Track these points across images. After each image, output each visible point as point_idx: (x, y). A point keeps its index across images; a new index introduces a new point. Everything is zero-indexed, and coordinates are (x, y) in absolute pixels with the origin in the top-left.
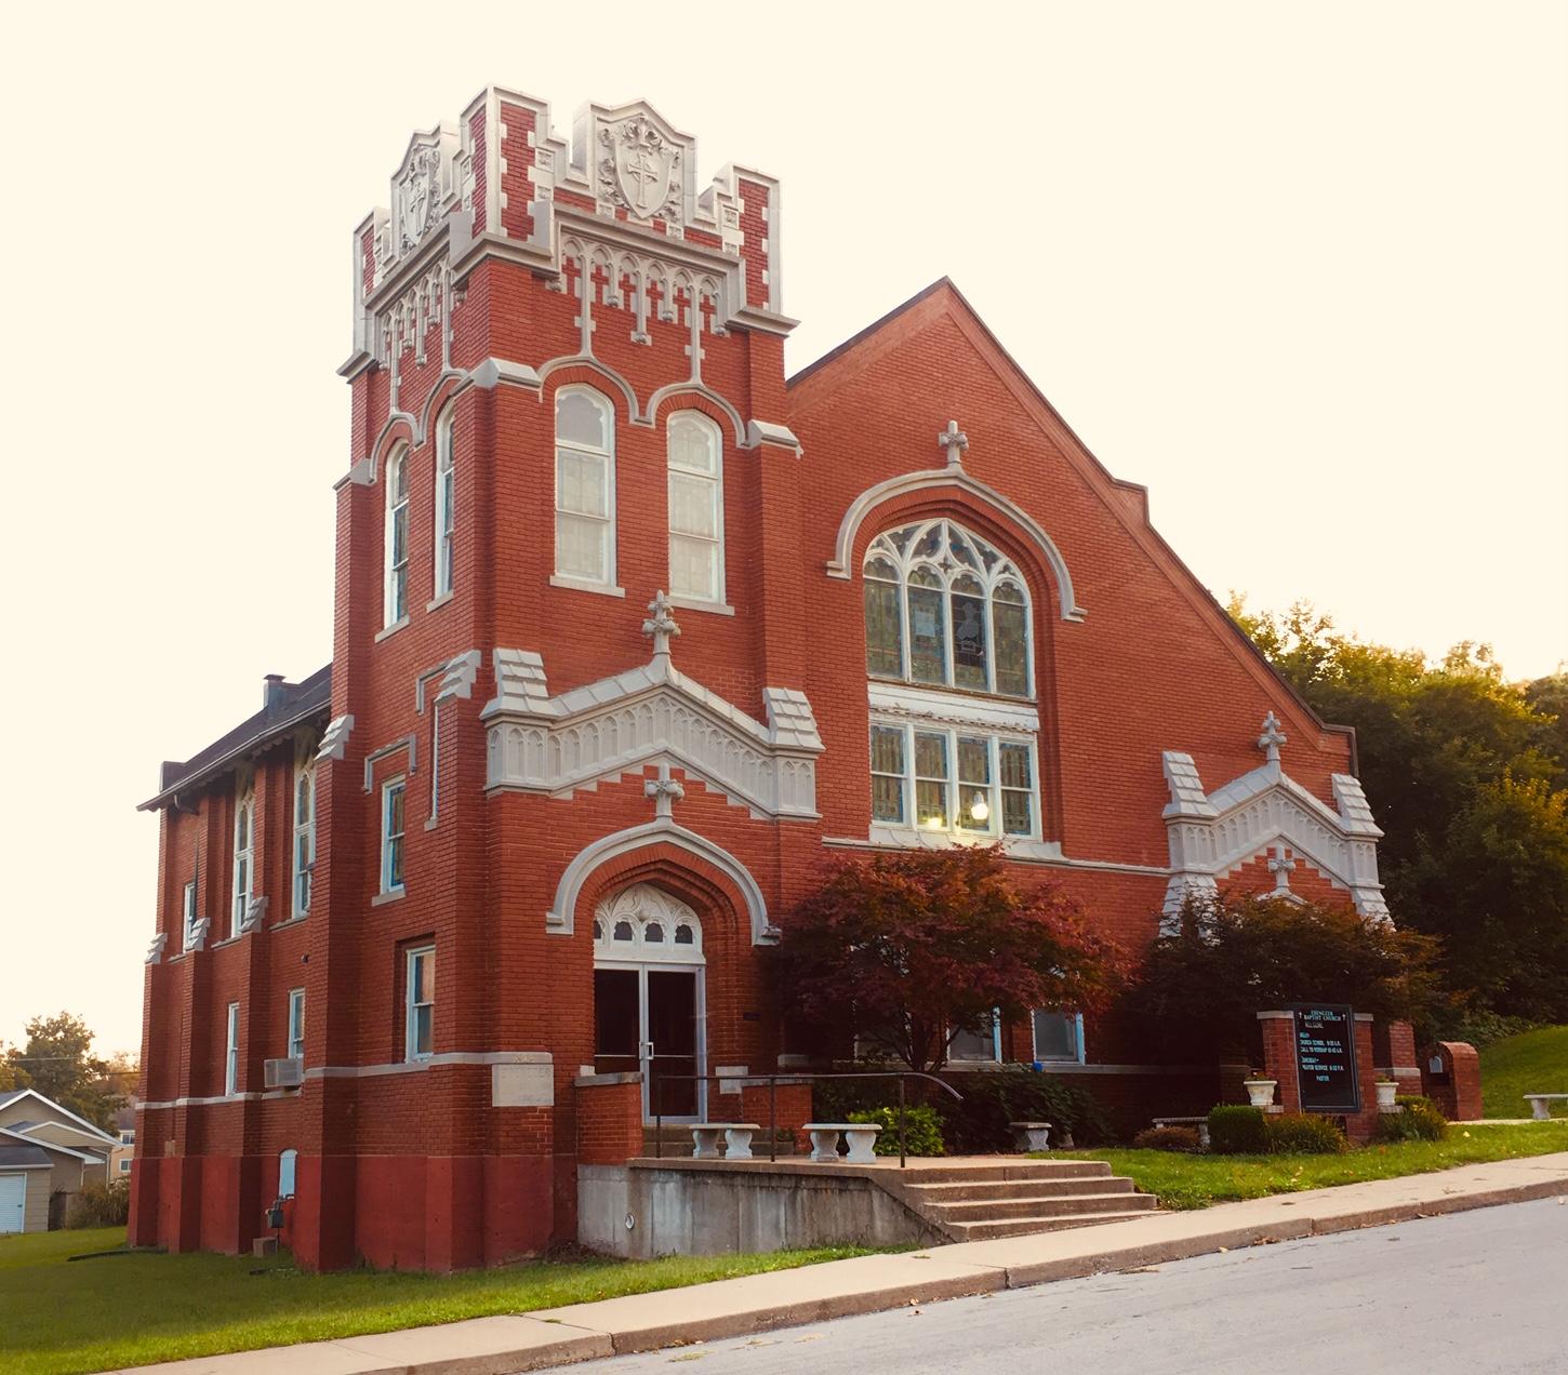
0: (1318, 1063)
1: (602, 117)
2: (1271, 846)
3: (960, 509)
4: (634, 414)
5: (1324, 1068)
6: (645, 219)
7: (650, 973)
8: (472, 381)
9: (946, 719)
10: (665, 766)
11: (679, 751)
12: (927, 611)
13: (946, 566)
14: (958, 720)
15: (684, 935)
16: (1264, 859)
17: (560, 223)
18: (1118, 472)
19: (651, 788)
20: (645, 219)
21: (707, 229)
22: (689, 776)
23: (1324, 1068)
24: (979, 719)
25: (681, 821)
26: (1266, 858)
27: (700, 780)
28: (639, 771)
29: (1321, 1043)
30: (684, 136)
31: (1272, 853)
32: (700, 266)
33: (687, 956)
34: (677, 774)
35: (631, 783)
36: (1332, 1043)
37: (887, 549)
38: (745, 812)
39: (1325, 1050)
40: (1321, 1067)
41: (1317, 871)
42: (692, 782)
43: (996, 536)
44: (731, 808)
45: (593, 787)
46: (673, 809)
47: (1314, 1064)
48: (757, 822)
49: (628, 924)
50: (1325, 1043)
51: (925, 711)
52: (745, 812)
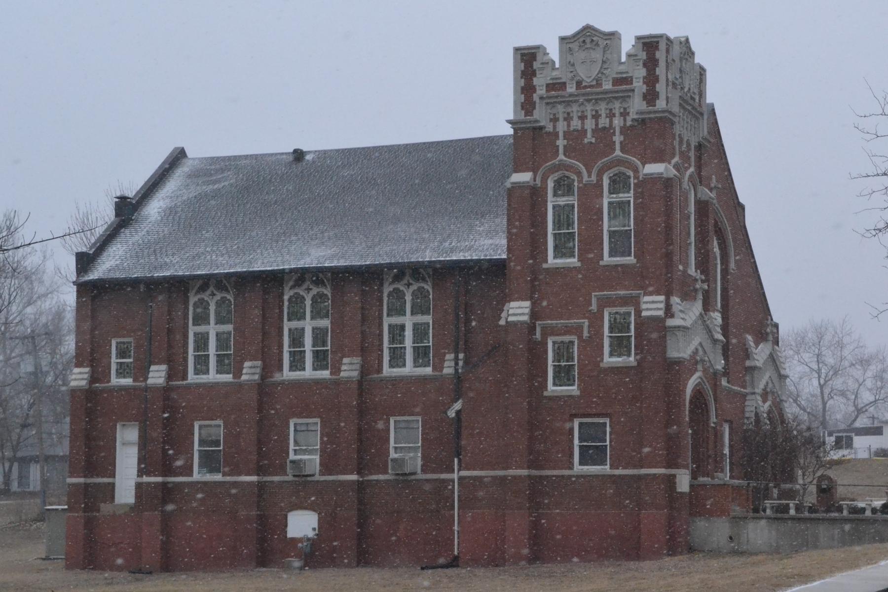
6: (591, 81)
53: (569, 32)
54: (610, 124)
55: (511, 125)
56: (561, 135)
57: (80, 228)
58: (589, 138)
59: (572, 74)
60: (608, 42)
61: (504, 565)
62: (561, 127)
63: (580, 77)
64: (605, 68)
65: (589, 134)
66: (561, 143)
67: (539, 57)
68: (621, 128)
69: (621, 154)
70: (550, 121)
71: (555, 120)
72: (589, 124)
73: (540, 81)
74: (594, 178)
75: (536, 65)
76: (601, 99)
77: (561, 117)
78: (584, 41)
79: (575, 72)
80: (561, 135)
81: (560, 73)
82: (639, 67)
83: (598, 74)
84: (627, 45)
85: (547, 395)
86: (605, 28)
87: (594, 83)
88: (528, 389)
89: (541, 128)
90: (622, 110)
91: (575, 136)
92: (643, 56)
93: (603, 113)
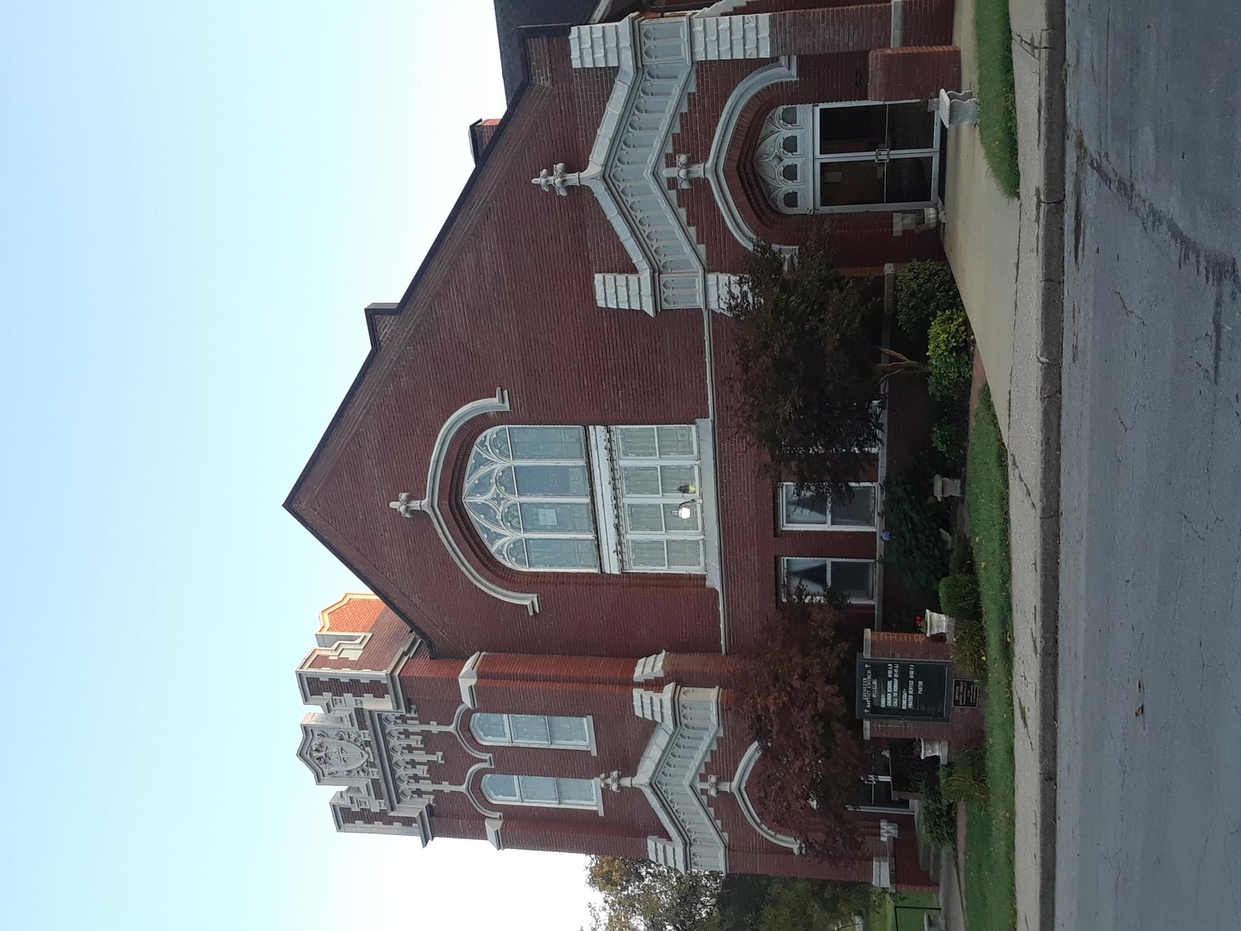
0: (907, 691)
1: (321, 774)
2: (665, 185)
3: (453, 497)
4: (486, 765)
5: (911, 683)
6: (368, 753)
7: (821, 163)
8: (497, 831)
9: (616, 513)
10: (666, 173)
11: (651, 160)
12: (537, 515)
13: (498, 499)
14: (615, 502)
15: (790, 119)
16: (681, 193)
17: (397, 805)
18: (364, 347)
19: (713, 793)
20: (368, 753)
21: (354, 717)
22: (670, 150)
23: (911, 683)
24: (610, 483)
25: (731, 776)
26: (678, 191)
27: (671, 138)
28: (673, 194)
29: (890, 683)
30: (304, 694)
31: (673, 183)
32: (380, 726)
33: (808, 120)
34: (671, 162)
35: (684, 199)
36: (890, 672)
37: (503, 546)
38: (718, 739)
39: (896, 681)
40: (911, 688)
41: (706, 763)
42: (706, 770)
43: (462, 517)
44: (718, 748)
45: (719, 823)
46: (698, 163)
47: (908, 694)
48: (725, 732)
49: (784, 148)
50: (890, 679)
51: (613, 530)
52: (718, 739)
53: (310, 776)
54: (418, 735)
55: (430, 841)
56: (425, 727)
57: (636, 199)
58: (438, 757)
59: (361, 772)
60: (315, 734)
61: (983, 732)
62: (427, 786)
63: (363, 764)
64: (349, 737)
65: (433, 758)
66: (446, 787)
67: (346, 803)
68: (421, 723)
69: (453, 725)
70: (415, 767)
71: (419, 793)
72: (420, 756)
73: (375, 806)
74: (487, 756)
75: (355, 809)
76: (390, 760)
77: (408, 757)
78: (317, 759)
79: (359, 769)
80: (425, 727)
81: (363, 782)
82: (343, 700)
83: (357, 745)
84: (314, 712)
85: (754, 743)
86: (299, 736)
87: (368, 749)
88: (826, 360)
89: (429, 807)
90: (403, 736)
91: (436, 773)
92: (328, 696)
93: (411, 772)
